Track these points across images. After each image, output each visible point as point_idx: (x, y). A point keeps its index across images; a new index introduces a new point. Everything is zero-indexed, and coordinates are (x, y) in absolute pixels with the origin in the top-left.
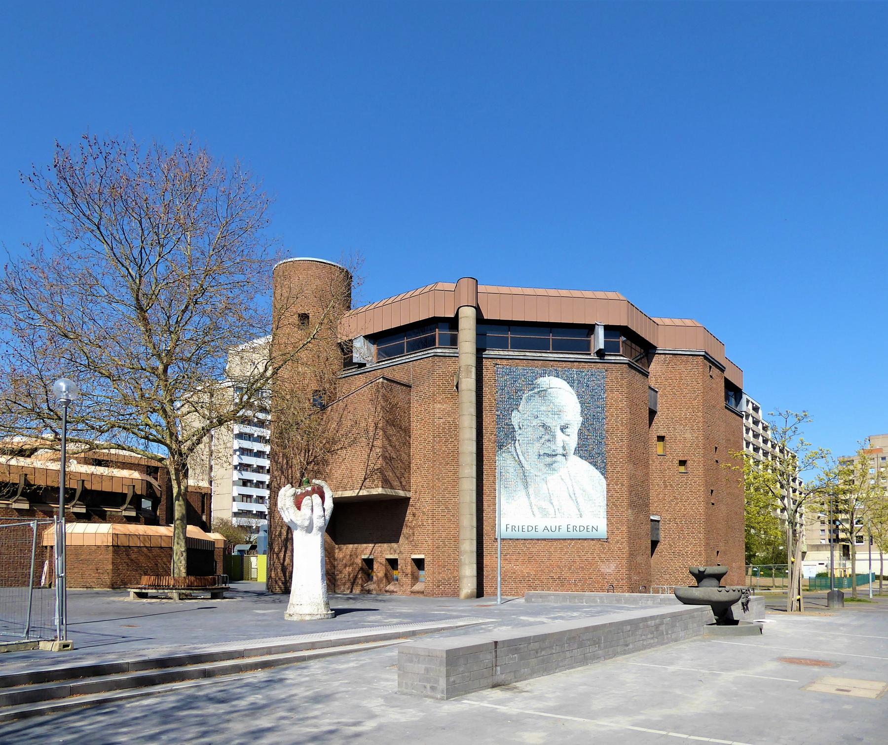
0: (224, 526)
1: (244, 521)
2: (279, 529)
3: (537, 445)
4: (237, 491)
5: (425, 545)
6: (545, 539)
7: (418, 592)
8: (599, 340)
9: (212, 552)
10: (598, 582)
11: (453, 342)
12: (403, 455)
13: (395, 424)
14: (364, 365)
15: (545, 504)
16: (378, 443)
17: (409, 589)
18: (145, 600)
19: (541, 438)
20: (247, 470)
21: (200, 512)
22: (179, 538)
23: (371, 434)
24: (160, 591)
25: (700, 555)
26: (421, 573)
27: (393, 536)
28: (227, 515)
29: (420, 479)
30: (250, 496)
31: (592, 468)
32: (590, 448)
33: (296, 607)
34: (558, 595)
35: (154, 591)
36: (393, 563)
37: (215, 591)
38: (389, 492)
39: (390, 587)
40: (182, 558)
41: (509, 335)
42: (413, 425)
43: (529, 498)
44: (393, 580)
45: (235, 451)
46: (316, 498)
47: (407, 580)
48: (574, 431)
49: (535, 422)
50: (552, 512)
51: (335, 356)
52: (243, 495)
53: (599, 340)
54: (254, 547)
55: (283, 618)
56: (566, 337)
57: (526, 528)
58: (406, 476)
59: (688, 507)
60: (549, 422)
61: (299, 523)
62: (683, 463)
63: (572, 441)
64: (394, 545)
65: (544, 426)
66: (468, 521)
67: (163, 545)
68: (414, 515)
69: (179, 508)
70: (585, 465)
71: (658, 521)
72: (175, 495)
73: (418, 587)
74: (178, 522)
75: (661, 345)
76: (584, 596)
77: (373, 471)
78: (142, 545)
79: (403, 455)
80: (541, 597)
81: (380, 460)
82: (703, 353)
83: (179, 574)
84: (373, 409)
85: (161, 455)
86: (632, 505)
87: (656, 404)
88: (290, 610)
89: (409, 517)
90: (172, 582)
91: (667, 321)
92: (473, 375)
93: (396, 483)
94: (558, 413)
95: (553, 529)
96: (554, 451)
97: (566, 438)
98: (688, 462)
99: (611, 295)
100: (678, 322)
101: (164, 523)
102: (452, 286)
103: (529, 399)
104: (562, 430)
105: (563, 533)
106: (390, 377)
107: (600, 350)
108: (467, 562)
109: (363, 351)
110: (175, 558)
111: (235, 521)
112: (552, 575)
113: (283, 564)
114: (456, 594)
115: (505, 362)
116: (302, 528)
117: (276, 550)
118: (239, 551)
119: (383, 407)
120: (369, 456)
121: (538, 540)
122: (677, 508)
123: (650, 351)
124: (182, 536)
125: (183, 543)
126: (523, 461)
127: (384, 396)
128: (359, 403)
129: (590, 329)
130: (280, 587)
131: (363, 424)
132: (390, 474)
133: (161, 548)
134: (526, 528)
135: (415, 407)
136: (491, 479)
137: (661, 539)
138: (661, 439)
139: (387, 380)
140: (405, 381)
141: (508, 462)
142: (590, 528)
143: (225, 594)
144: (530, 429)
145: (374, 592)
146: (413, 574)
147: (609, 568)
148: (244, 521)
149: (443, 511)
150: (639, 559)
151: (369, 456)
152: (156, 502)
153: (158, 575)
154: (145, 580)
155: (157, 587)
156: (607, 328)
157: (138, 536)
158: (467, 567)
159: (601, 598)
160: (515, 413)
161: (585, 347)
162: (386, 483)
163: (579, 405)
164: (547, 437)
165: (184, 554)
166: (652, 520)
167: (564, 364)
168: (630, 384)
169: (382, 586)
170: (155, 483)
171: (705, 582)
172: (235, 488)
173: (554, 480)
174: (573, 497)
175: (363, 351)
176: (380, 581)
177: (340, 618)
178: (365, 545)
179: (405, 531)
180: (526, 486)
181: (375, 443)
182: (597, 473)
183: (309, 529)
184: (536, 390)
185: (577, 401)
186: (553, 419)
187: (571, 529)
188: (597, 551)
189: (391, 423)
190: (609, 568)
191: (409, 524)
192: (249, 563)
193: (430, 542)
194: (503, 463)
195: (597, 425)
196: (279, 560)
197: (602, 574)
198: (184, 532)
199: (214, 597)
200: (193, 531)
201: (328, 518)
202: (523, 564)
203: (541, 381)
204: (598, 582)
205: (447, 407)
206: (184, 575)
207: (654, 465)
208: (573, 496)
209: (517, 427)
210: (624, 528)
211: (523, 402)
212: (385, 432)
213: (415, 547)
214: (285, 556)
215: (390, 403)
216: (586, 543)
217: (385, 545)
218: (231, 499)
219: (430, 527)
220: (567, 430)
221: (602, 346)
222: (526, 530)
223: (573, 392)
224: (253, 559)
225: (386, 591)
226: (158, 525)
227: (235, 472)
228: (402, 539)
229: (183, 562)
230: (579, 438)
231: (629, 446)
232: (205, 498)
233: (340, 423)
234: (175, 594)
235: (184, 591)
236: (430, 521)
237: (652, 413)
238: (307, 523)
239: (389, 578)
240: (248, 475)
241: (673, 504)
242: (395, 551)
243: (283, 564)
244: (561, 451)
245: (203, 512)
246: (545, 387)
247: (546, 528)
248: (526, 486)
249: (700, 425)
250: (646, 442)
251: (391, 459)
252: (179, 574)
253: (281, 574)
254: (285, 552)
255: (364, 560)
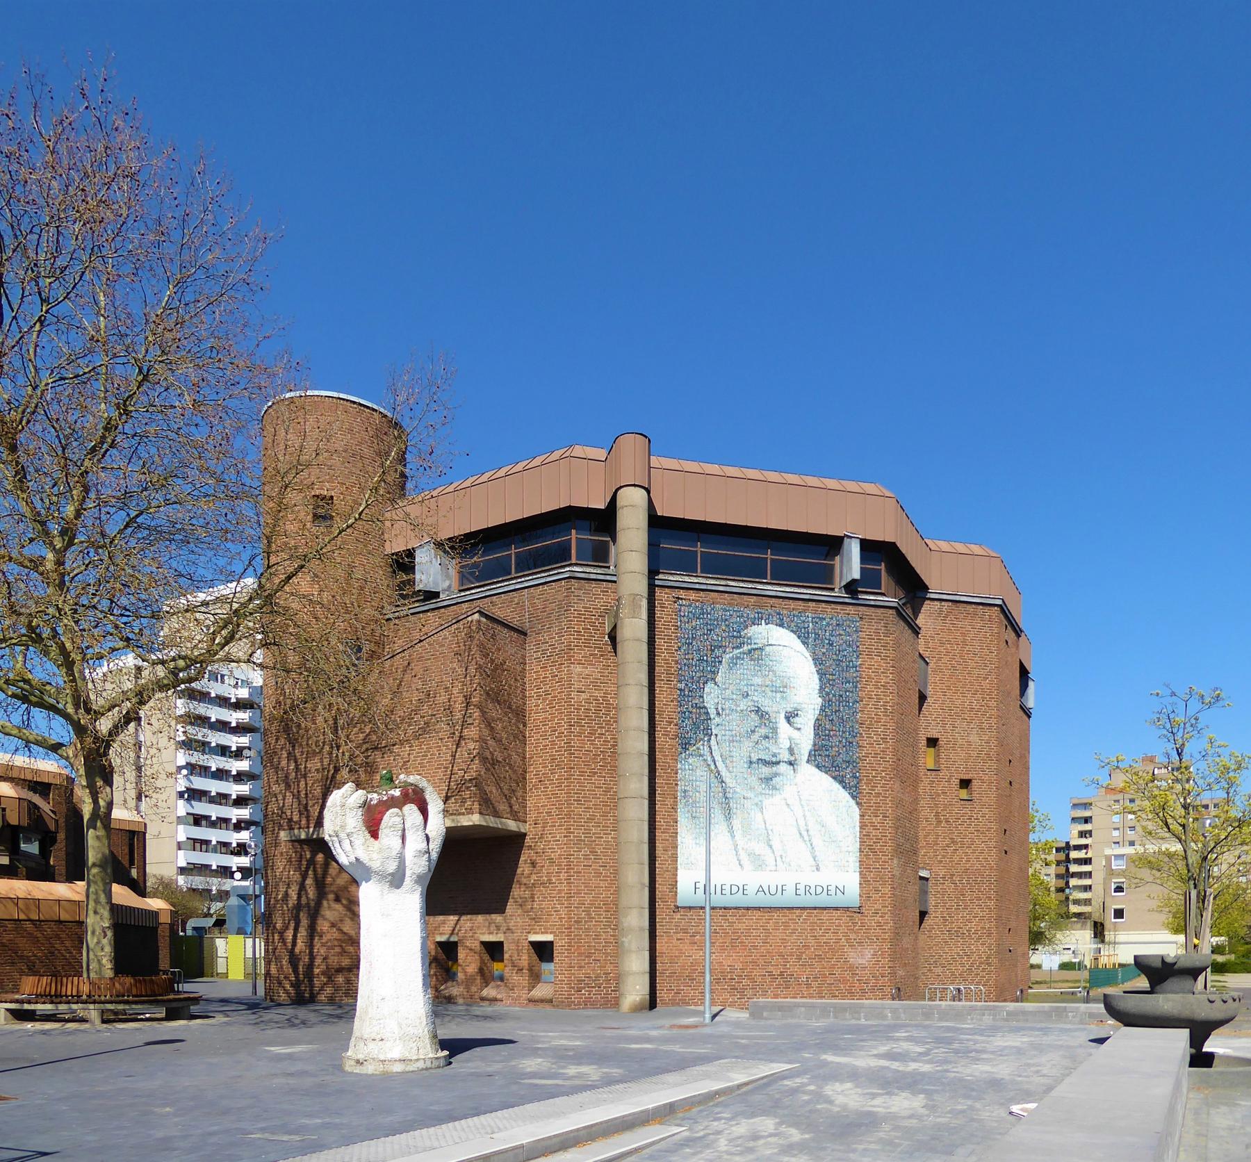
0: (166, 889)
1: (198, 882)
2: (282, 889)
3: (747, 744)
4: (183, 833)
5: (555, 917)
6: (758, 909)
7: (542, 1001)
8: (852, 564)
9: (154, 930)
10: (845, 981)
11: (600, 555)
12: (515, 756)
13: (501, 700)
14: (435, 595)
15: (760, 848)
16: (472, 732)
17: (524, 994)
18: (29, 1026)
19: (753, 731)
20: (200, 800)
21: (126, 862)
22: (97, 902)
23: (458, 715)
24: (62, 1007)
25: (989, 935)
26: (546, 967)
27: (495, 902)
28: (169, 872)
29: (544, 801)
30: (207, 842)
31: (837, 786)
32: (834, 753)
33: (371, 1045)
34: (813, 1006)
35: (49, 1006)
36: (494, 950)
37: (174, 1005)
38: (492, 822)
39: (489, 992)
40: (105, 941)
41: (699, 549)
42: (531, 703)
43: (733, 836)
44: (493, 979)
45: (180, 768)
46: (411, 810)
47: (521, 980)
48: (807, 721)
49: (743, 704)
50: (770, 860)
51: (382, 579)
52: (195, 840)
53: (852, 564)
54: (220, 923)
55: (339, 1068)
56: (798, 556)
57: (727, 888)
58: (519, 794)
59: (972, 857)
60: (767, 704)
61: (375, 865)
62: (965, 784)
63: (806, 740)
64: (497, 918)
65: (758, 711)
66: (635, 875)
67: (64, 916)
68: (533, 864)
69: (97, 844)
70: (825, 782)
71: (927, 879)
72: (86, 817)
73: (541, 991)
74: (95, 871)
75: (935, 589)
76: (862, 1006)
77: (462, 785)
78: (22, 917)
79: (515, 756)
80: (781, 1008)
81: (476, 765)
82: (999, 602)
83: (99, 972)
84: (461, 671)
85: (54, 739)
86: (899, 851)
87: (926, 684)
88: (355, 1051)
89: (523, 868)
90: (85, 989)
91: (944, 546)
92: (644, 615)
93: (503, 807)
94: (781, 689)
95: (773, 891)
96: (774, 755)
97: (795, 734)
98: (974, 783)
99: (870, 488)
100: (960, 548)
101: (61, 869)
102: (601, 454)
103: (734, 662)
104: (788, 719)
105: (789, 899)
106: (498, 613)
107: (854, 581)
108: (634, 947)
109: (432, 571)
110: (91, 940)
111: (181, 880)
112: (770, 968)
113: (292, 952)
114: (612, 1002)
115: (693, 595)
116: (382, 876)
117: (279, 926)
118: (194, 929)
119: (480, 667)
120: (454, 756)
121: (748, 909)
122: (956, 858)
123: (920, 594)
124: (103, 898)
125: (106, 913)
126: (724, 773)
127: (481, 646)
128: (434, 663)
129: (833, 545)
130: (286, 992)
131: (442, 698)
132: (492, 790)
133: (60, 922)
134: (727, 888)
135: (534, 671)
136: (669, 802)
137: (931, 909)
138: (932, 742)
139: (487, 616)
140: (515, 623)
141: (699, 773)
142: (832, 888)
143: (194, 1009)
144: (734, 716)
145: (460, 1001)
146: (530, 970)
147: (863, 957)
148: (198, 882)
149: (586, 857)
150: (907, 942)
151: (454, 756)
152: (47, 841)
153: (55, 975)
154: (29, 985)
155: (55, 998)
156: (870, 549)
157: (15, 901)
158: (634, 956)
159: (894, 1011)
160: (709, 687)
161: (823, 577)
162: (487, 805)
163: (816, 677)
164: (763, 731)
165: (110, 934)
166: (921, 878)
167: (792, 604)
168: (898, 644)
169: (474, 989)
170: (45, 807)
171: (1172, 983)
172: (181, 828)
173: (773, 804)
174: (804, 835)
175: (432, 571)
176: (469, 982)
177: (467, 1062)
178: (441, 918)
179: (516, 892)
180: (728, 814)
181: (465, 732)
182: (844, 795)
183: (396, 880)
184: (746, 648)
185: (814, 670)
186: (772, 698)
187: (801, 892)
188: (843, 929)
189: (494, 696)
190: (863, 957)
191: (524, 880)
192: (214, 949)
193: (563, 913)
194: (691, 773)
195: (845, 713)
196: (284, 943)
197: (851, 968)
198: (109, 894)
199: (172, 1015)
200: (122, 895)
201: (434, 856)
202: (723, 949)
203: (753, 631)
204: (845, 981)
205: (593, 671)
206: (109, 973)
207: (924, 786)
208: (804, 833)
209: (712, 712)
210: (887, 890)
211: (723, 669)
212: (483, 713)
213: (536, 921)
214: (295, 936)
215: (492, 661)
216: (825, 915)
217: (480, 918)
218: (175, 846)
219: (564, 887)
220: (796, 720)
221: (856, 575)
222: (727, 891)
223: (807, 654)
224: (220, 943)
225: (483, 999)
226: (54, 881)
227: (181, 803)
228: (510, 907)
229: (108, 949)
230: (816, 734)
231: (895, 751)
232: (134, 839)
233: (396, 693)
234: (93, 1013)
235: (109, 1006)
236: (563, 876)
237: (922, 698)
238: (392, 867)
239: (485, 976)
240: (201, 808)
241: (950, 850)
242: (498, 928)
243: (292, 952)
244: (785, 756)
245: (132, 863)
246: (760, 642)
247: (761, 889)
248: (728, 814)
249: (993, 721)
250: (914, 745)
251: (494, 762)
252: (99, 972)
253: (287, 969)
254: (296, 930)
255: (440, 944)
